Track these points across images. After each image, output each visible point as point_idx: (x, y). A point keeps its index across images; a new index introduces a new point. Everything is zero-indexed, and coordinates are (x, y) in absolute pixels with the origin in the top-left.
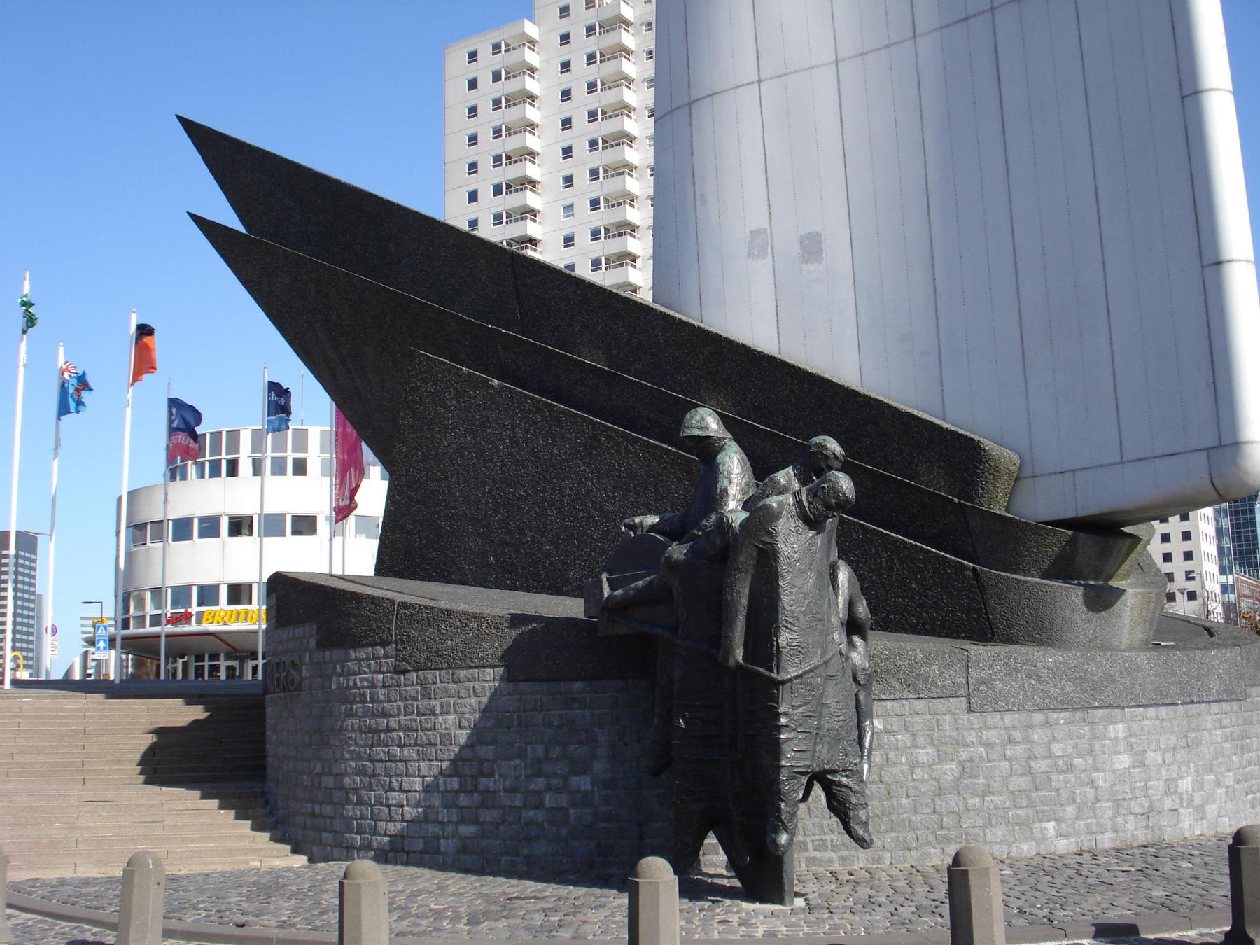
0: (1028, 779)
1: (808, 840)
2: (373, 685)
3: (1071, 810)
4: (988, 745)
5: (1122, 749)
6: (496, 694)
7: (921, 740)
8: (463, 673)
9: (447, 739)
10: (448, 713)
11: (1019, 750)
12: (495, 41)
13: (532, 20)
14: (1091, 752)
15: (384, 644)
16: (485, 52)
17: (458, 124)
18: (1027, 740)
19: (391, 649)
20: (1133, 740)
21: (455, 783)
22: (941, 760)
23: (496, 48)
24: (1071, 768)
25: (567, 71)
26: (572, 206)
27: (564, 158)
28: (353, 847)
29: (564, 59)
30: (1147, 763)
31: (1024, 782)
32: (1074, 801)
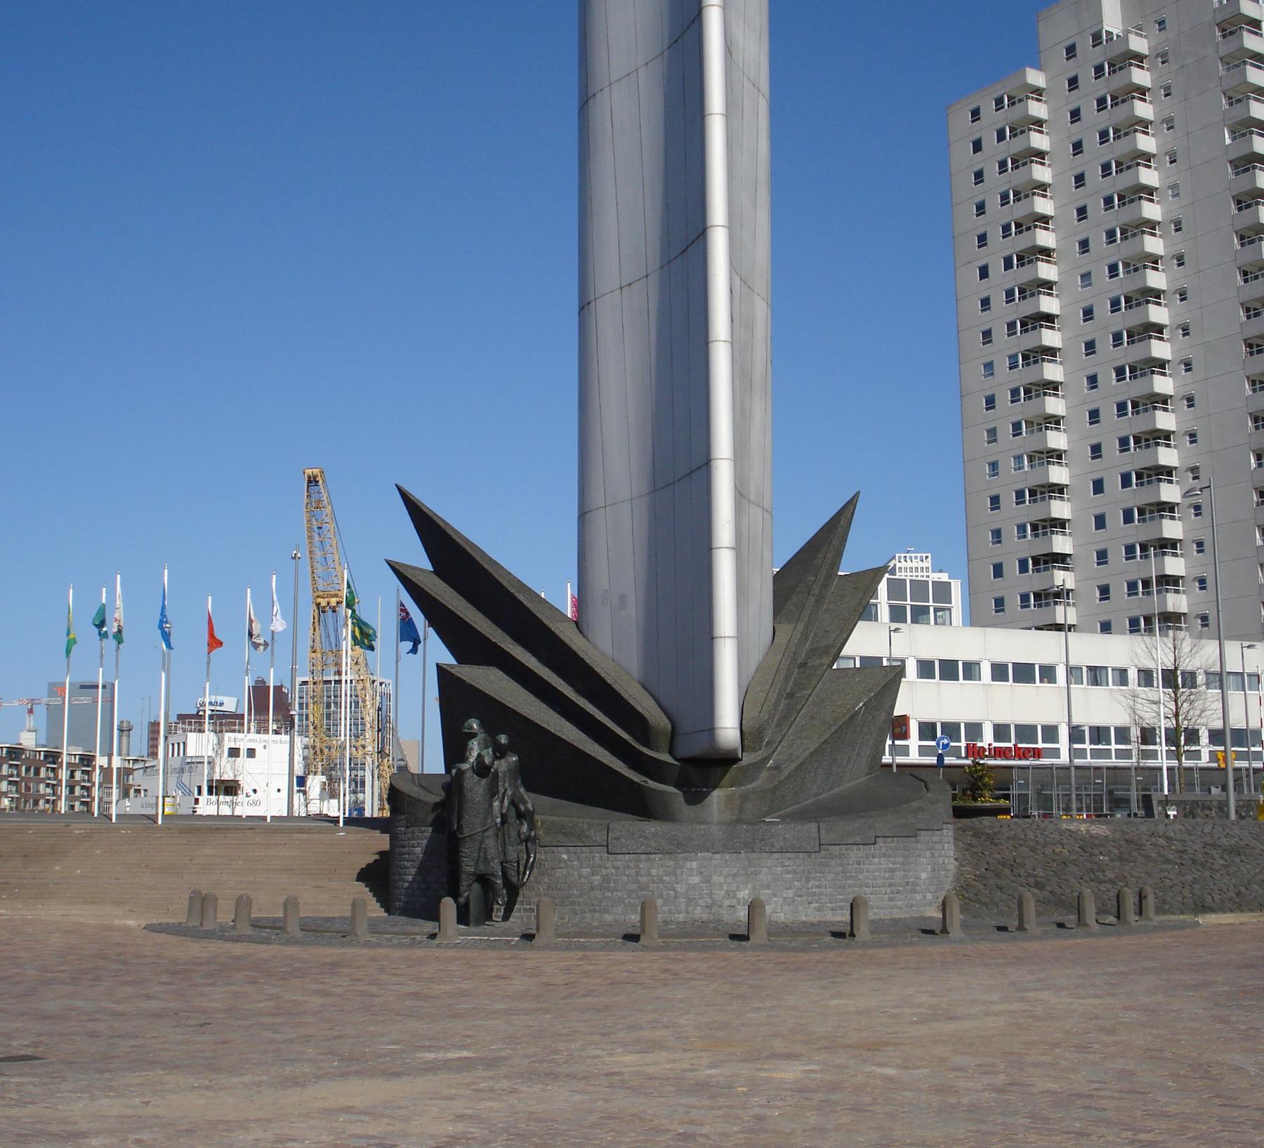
0: (637, 885)
4: (616, 868)
5: (695, 873)
8: (423, 828)
11: (632, 872)
12: (997, 95)
13: (1038, 66)
14: (674, 874)
15: (404, 814)
16: (988, 107)
17: (967, 192)
18: (637, 867)
19: (406, 815)
20: (703, 870)
23: (999, 102)
24: (661, 881)
29: (1073, 106)
31: (633, 887)
32: (662, 897)
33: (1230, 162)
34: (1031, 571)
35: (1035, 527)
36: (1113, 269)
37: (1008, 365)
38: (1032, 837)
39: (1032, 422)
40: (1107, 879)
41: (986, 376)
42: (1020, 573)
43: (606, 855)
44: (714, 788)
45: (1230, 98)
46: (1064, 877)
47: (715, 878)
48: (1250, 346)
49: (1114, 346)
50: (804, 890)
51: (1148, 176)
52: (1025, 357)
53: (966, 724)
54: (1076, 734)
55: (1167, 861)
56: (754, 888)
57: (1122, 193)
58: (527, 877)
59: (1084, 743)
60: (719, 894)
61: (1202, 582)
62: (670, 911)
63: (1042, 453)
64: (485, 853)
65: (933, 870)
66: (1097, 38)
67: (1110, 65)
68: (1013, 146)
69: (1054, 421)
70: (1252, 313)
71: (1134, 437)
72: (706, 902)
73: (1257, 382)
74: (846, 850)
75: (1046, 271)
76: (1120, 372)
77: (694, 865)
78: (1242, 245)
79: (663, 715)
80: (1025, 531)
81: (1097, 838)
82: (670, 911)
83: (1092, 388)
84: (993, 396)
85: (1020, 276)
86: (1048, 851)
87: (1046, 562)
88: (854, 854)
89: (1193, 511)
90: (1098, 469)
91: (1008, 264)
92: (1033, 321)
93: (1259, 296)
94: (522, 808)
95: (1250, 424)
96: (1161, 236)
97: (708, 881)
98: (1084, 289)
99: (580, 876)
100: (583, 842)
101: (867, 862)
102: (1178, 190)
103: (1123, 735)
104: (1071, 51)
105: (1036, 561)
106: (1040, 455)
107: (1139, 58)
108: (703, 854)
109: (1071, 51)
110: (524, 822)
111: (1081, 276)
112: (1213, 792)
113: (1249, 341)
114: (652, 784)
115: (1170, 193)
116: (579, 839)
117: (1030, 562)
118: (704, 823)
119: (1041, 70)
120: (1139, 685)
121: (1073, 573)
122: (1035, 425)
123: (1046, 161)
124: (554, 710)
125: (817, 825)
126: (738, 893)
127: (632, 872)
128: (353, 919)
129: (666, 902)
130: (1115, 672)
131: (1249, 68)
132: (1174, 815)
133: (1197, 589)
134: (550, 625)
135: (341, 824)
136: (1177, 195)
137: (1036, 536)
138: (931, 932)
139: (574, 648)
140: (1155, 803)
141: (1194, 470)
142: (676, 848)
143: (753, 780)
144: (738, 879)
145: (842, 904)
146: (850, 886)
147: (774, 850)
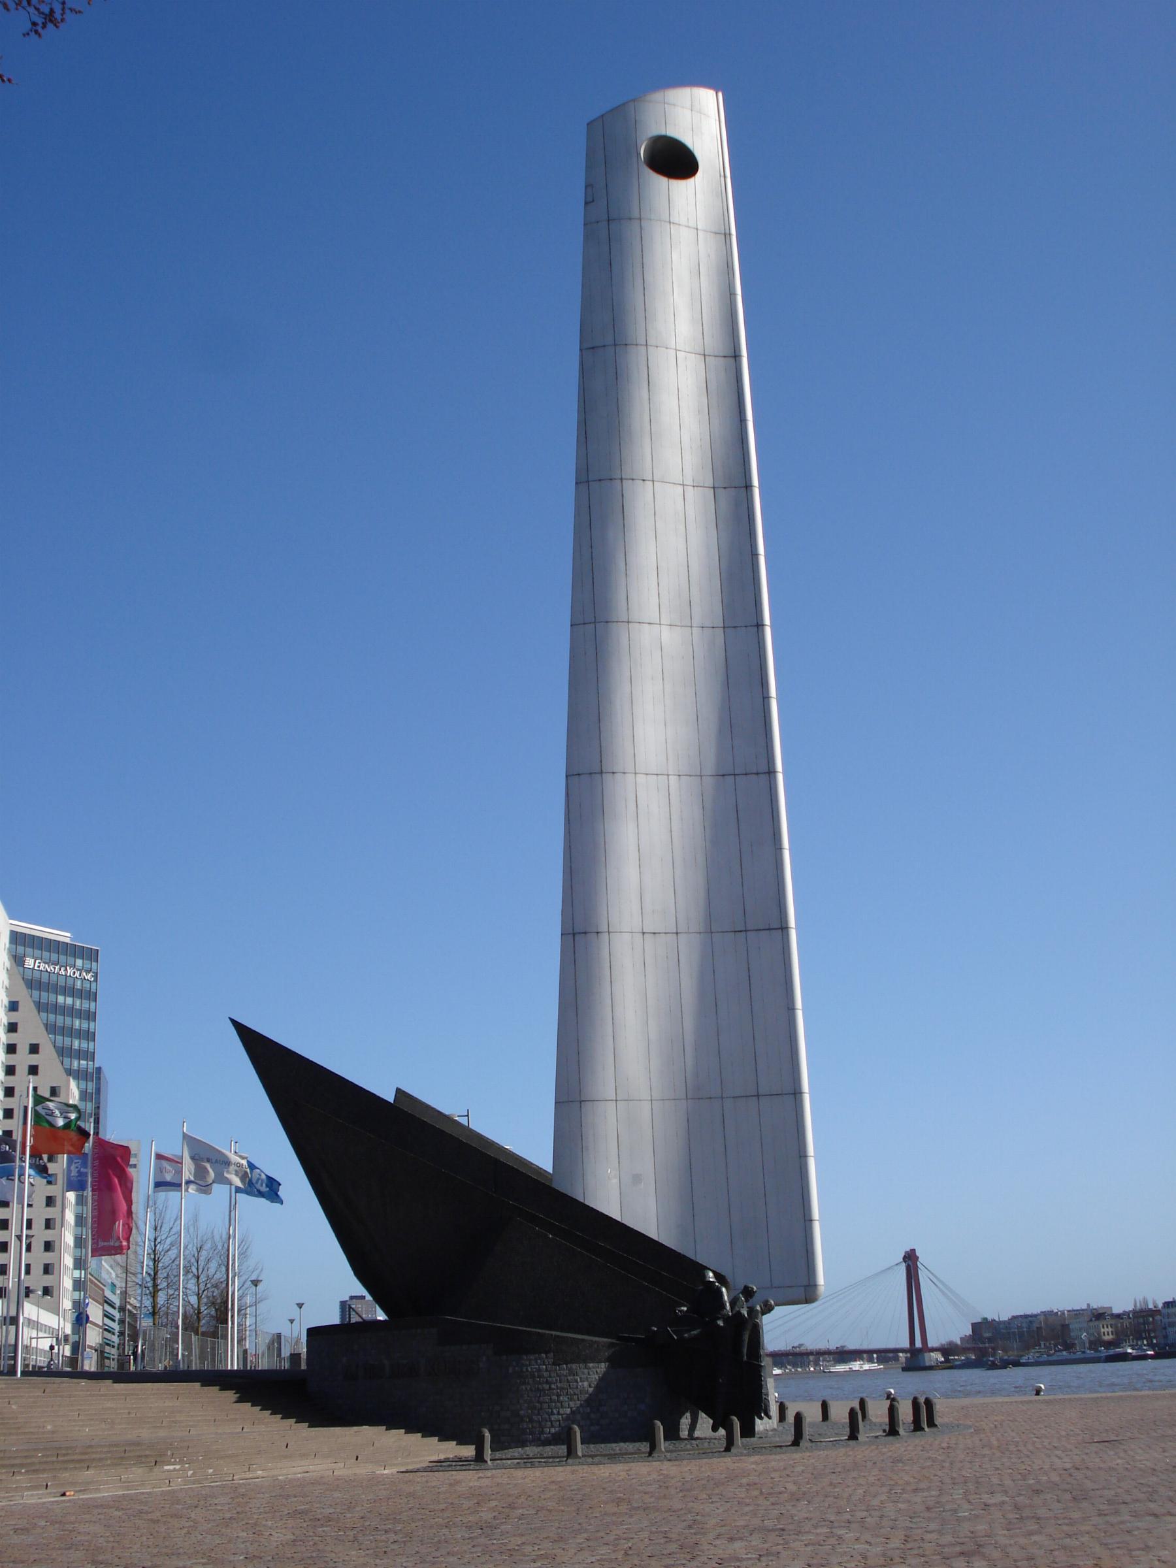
6: (605, 1374)
9: (583, 1391)
10: (584, 1381)
21: (588, 1410)
28: (527, 1441)
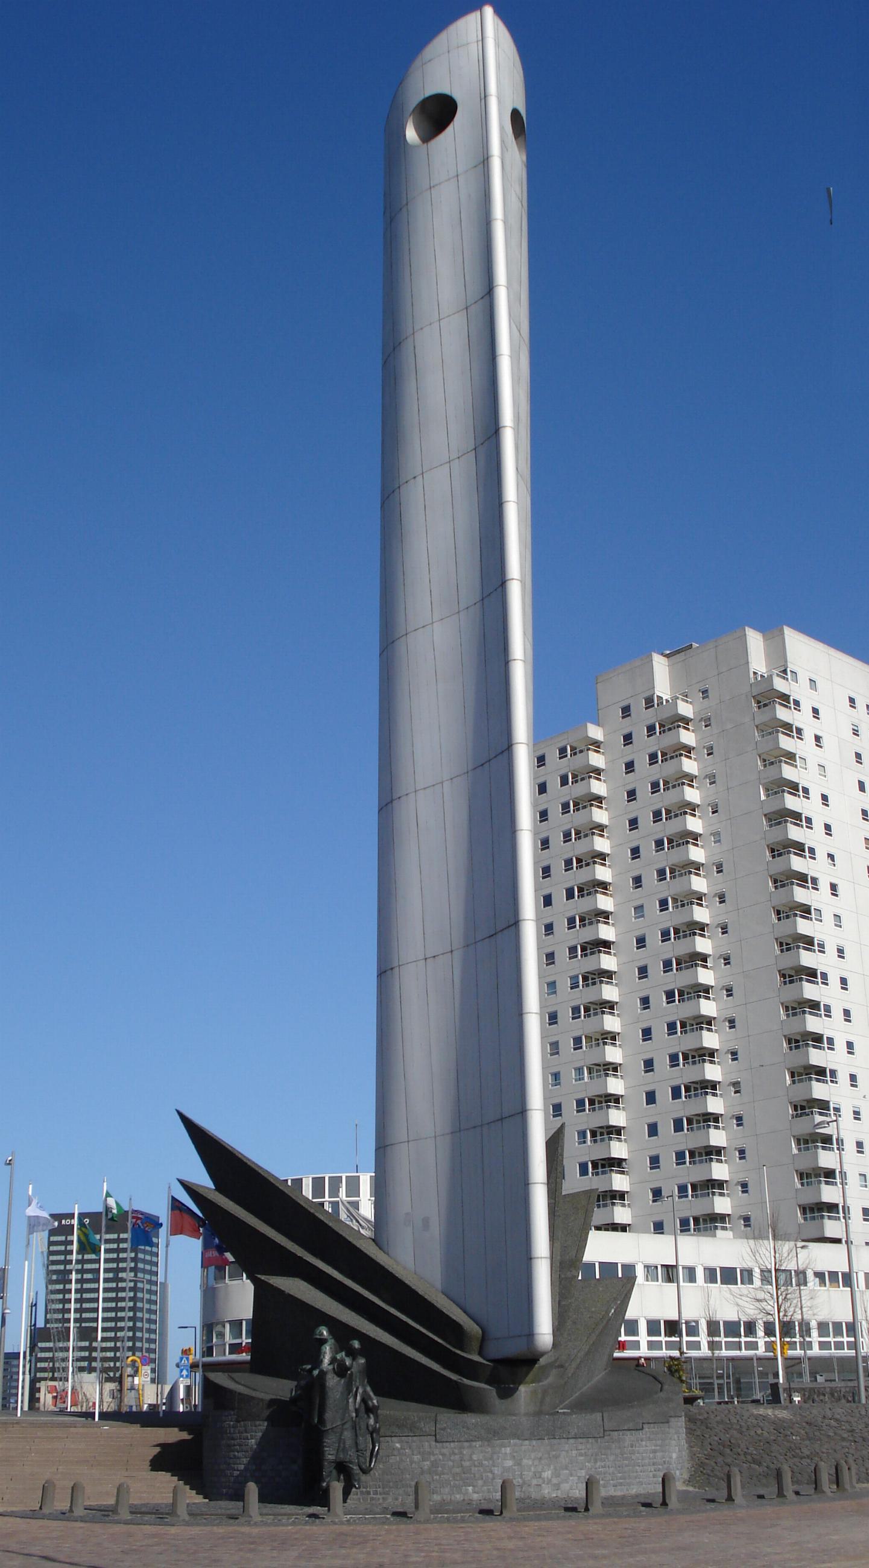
0: (460, 1469)
1: (371, 1490)
2: (229, 1427)
3: (480, 1482)
4: (443, 1455)
7: (415, 1452)
8: (258, 1423)
11: (457, 1457)
14: (491, 1458)
15: (233, 1409)
18: (461, 1453)
20: (515, 1454)
22: (423, 1460)
23: (563, 751)
24: (481, 1465)
25: (631, 772)
26: (642, 906)
27: (633, 859)
29: (628, 759)
30: (523, 1464)
32: (482, 1479)
33: (765, 815)
34: (590, 1174)
35: (594, 1134)
36: (663, 904)
37: (569, 985)
38: (736, 1422)
39: (591, 1037)
40: (805, 1455)
41: (548, 994)
42: (580, 1176)
43: (434, 1443)
44: (520, 1384)
45: (765, 761)
46: (773, 1454)
47: (525, 1462)
48: (784, 976)
49: (664, 972)
50: (593, 1470)
51: (694, 824)
52: (585, 979)
53: (665, 1321)
54: (713, 1327)
55: (843, 1439)
56: (555, 1469)
57: (671, 837)
58: (373, 1464)
59: (660, 1335)
60: (527, 1475)
61: (744, 1186)
62: (489, 1491)
63: (599, 1065)
64: (344, 1443)
65: (679, 1451)
66: (649, 702)
67: (661, 726)
68: (576, 790)
69: (611, 1037)
70: (785, 947)
71: (682, 1053)
72: (518, 1482)
73: (790, 1009)
74: (623, 1435)
75: (604, 902)
76: (670, 995)
77: (508, 1450)
78: (776, 888)
79: (472, 1322)
80: (585, 1137)
81: (784, 1422)
82: (489, 1491)
83: (645, 1009)
84: (556, 1012)
85: (580, 906)
86: (752, 1433)
87: (603, 1166)
88: (629, 1438)
89: (735, 1121)
90: (650, 1081)
91: (570, 894)
92: (592, 947)
93: (792, 933)
94: (370, 1403)
95: (785, 1045)
96: (704, 877)
97: (519, 1464)
98: (637, 920)
99: (412, 1462)
100: (414, 1433)
101: (637, 1445)
102: (720, 837)
103: (750, 1328)
104: (626, 711)
105: (595, 1165)
106: (598, 1067)
107: (686, 721)
108: (515, 1441)
109: (626, 711)
110: (371, 1416)
111: (635, 909)
112: (818, 1380)
113: (782, 972)
114: (466, 1381)
115: (713, 839)
116: (410, 1429)
117: (590, 1165)
118: (514, 1415)
119: (599, 726)
120: (647, 1281)
121: (628, 1177)
122: (593, 1040)
123: (603, 805)
124: (363, 1317)
125: (601, 1414)
126: (543, 1473)
127: (457, 1457)
128: (174, 1504)
129: (485, 1483)
130: (685, 1270)
131: (781, 736)
132: (799, 1401)
133: (740, 1192)
134: (354, 1242)
135: (97, 1419)
136: (719, 841)
137: (595, 1141)
138: (574, 1509)
139: (382, 1263)
140: (781, 1390)
141: (736, 1084)
142: (495, 1434)
143: (547, 1378)
144: (543, 1462)
145: (621, 1481)
146: (626, 1466)
147: (570, 1436)
